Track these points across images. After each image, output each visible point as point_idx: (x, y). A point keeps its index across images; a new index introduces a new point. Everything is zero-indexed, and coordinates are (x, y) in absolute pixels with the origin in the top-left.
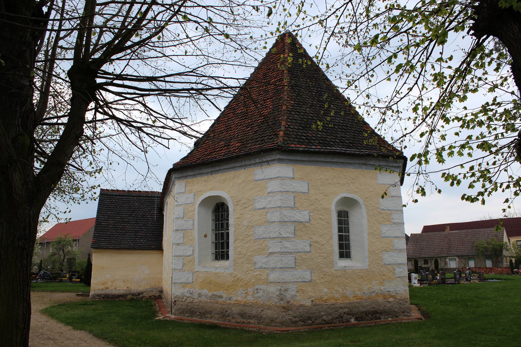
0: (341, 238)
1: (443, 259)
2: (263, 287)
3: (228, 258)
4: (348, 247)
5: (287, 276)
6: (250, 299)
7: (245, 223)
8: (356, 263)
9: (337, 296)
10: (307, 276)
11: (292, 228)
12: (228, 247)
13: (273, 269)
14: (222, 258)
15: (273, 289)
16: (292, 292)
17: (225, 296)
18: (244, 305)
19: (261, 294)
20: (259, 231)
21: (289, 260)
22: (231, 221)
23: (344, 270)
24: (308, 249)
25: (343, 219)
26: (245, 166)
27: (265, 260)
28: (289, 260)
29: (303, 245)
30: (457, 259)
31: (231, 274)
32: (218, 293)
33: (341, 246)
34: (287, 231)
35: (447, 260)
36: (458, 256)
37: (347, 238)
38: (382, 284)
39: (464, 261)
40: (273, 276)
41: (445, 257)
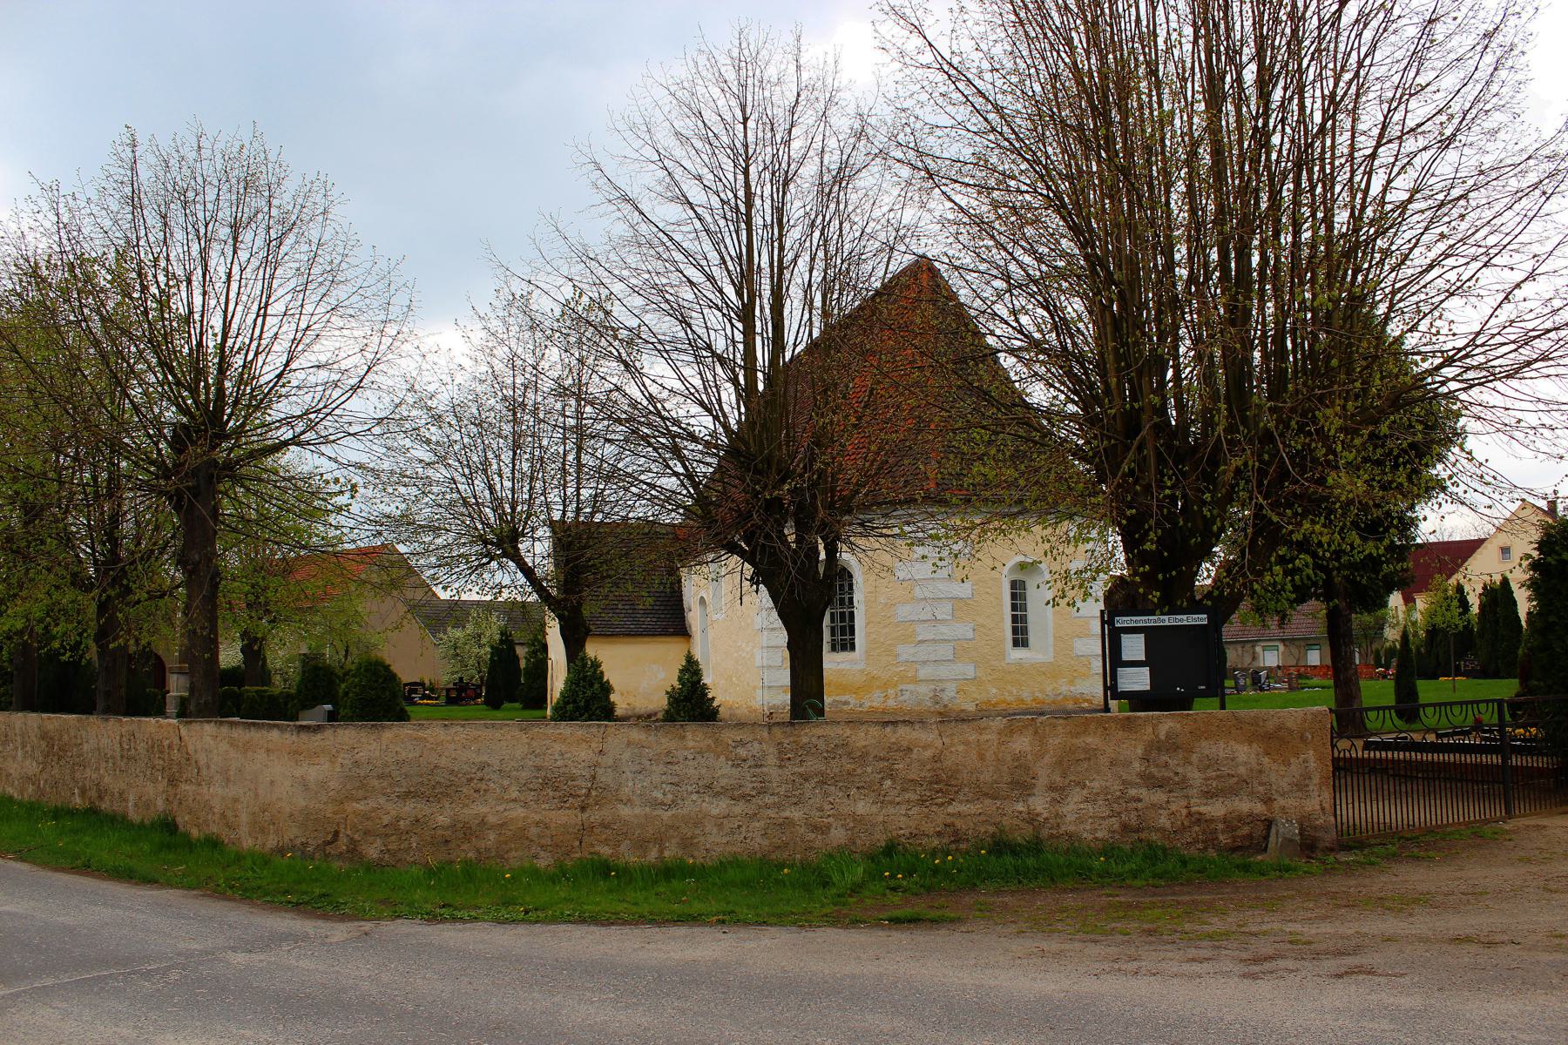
0: (1015, 619)
1: (1248, 646)
2: (911, 687)
3: (853, 648)
4: (1025, 631)
5: (943, 672)
6: (891, 703)
7: (882, 600)
8: (1038, 652)
9: (1010, 698)
10: (970, 671)
11: (949, 607)
12: (852, 632)
13: (924, 662)
14: (844, 648)
15: (924, 690)
16: (949, 693)
17: (852, 701)
18: (883, 712)
19: (907, 696)
20: (904, 612)
21: (946, 651)
22: (858, 597)
23: (1020, 664)
24: (970, 635)
25: (1018, 593)
26: (1042, 925)
27: (913, 651)
28: (946, 651)
29: (964, 630)
30: (1281, 648)
31: (862, 671)
32: (843, 698)
33: (1015, 631)
34: (944, 611)
35: (1258, 649)
36: (1283, 641)
37: (1024, 619)
38: (1071, 682)
39: (1295, 651)
40: (924, 672)
41: (1254, 643)
